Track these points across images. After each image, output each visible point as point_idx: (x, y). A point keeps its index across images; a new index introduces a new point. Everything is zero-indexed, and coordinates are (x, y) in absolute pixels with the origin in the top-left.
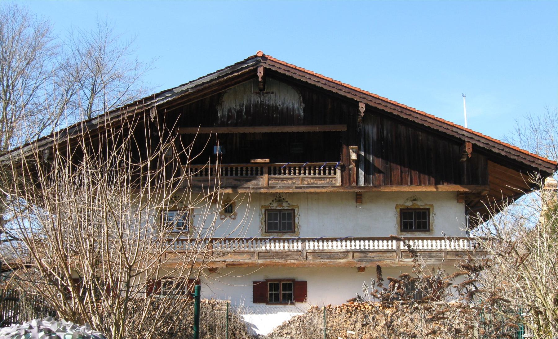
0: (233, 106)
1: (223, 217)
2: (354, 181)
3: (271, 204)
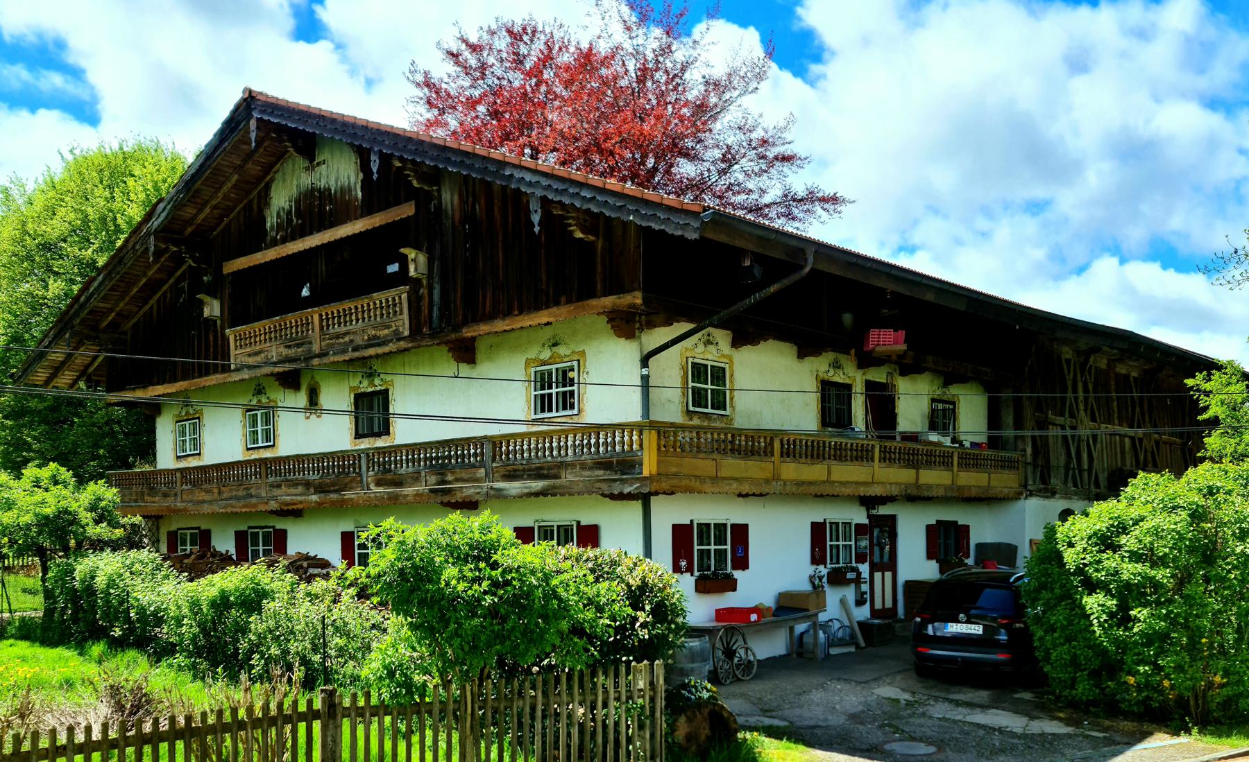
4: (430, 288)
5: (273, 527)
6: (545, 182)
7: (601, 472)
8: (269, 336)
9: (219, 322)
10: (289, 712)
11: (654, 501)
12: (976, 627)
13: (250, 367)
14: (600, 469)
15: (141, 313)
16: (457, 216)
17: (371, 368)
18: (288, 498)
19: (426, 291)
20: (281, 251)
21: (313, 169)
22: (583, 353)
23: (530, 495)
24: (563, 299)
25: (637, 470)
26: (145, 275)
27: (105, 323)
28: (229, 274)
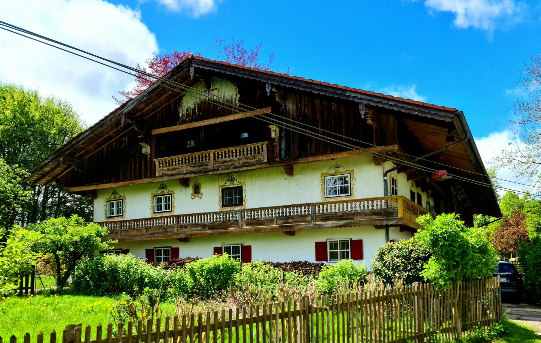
0: (189, 105)
1: (193, 197)
2: (277, 157)
3: (226, 183)
4: (280, 143)
5: (171, 247)
6: (369, 98)
7: (376, 217)
8: (186, 161)
9: (148, 156)
10: (205, 324)
11: (390, 229)
12: (504, 279)
13: (169, 175)
14: (375, 215)
15: (96, 151)
16: (295, 114)
17: (232, 177)
18: (192, 232)
19: (277, 144)
20: (189, 126)
21: (209, 91)
22: (353, 171)
23: (337, 227)
24: (113, 180)
25: (395, 215)
26: (108, 133)
27: (78, 155)
28: (155, 135)
